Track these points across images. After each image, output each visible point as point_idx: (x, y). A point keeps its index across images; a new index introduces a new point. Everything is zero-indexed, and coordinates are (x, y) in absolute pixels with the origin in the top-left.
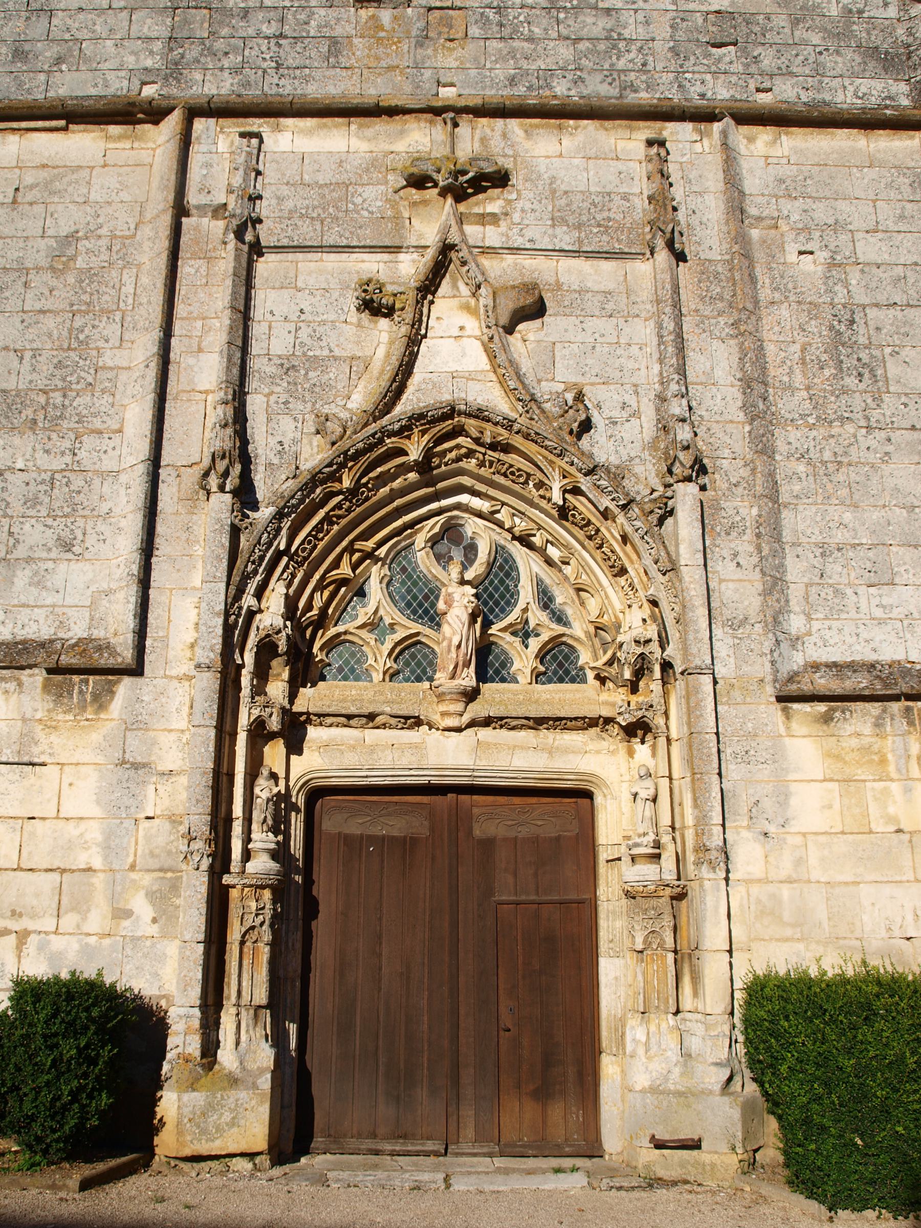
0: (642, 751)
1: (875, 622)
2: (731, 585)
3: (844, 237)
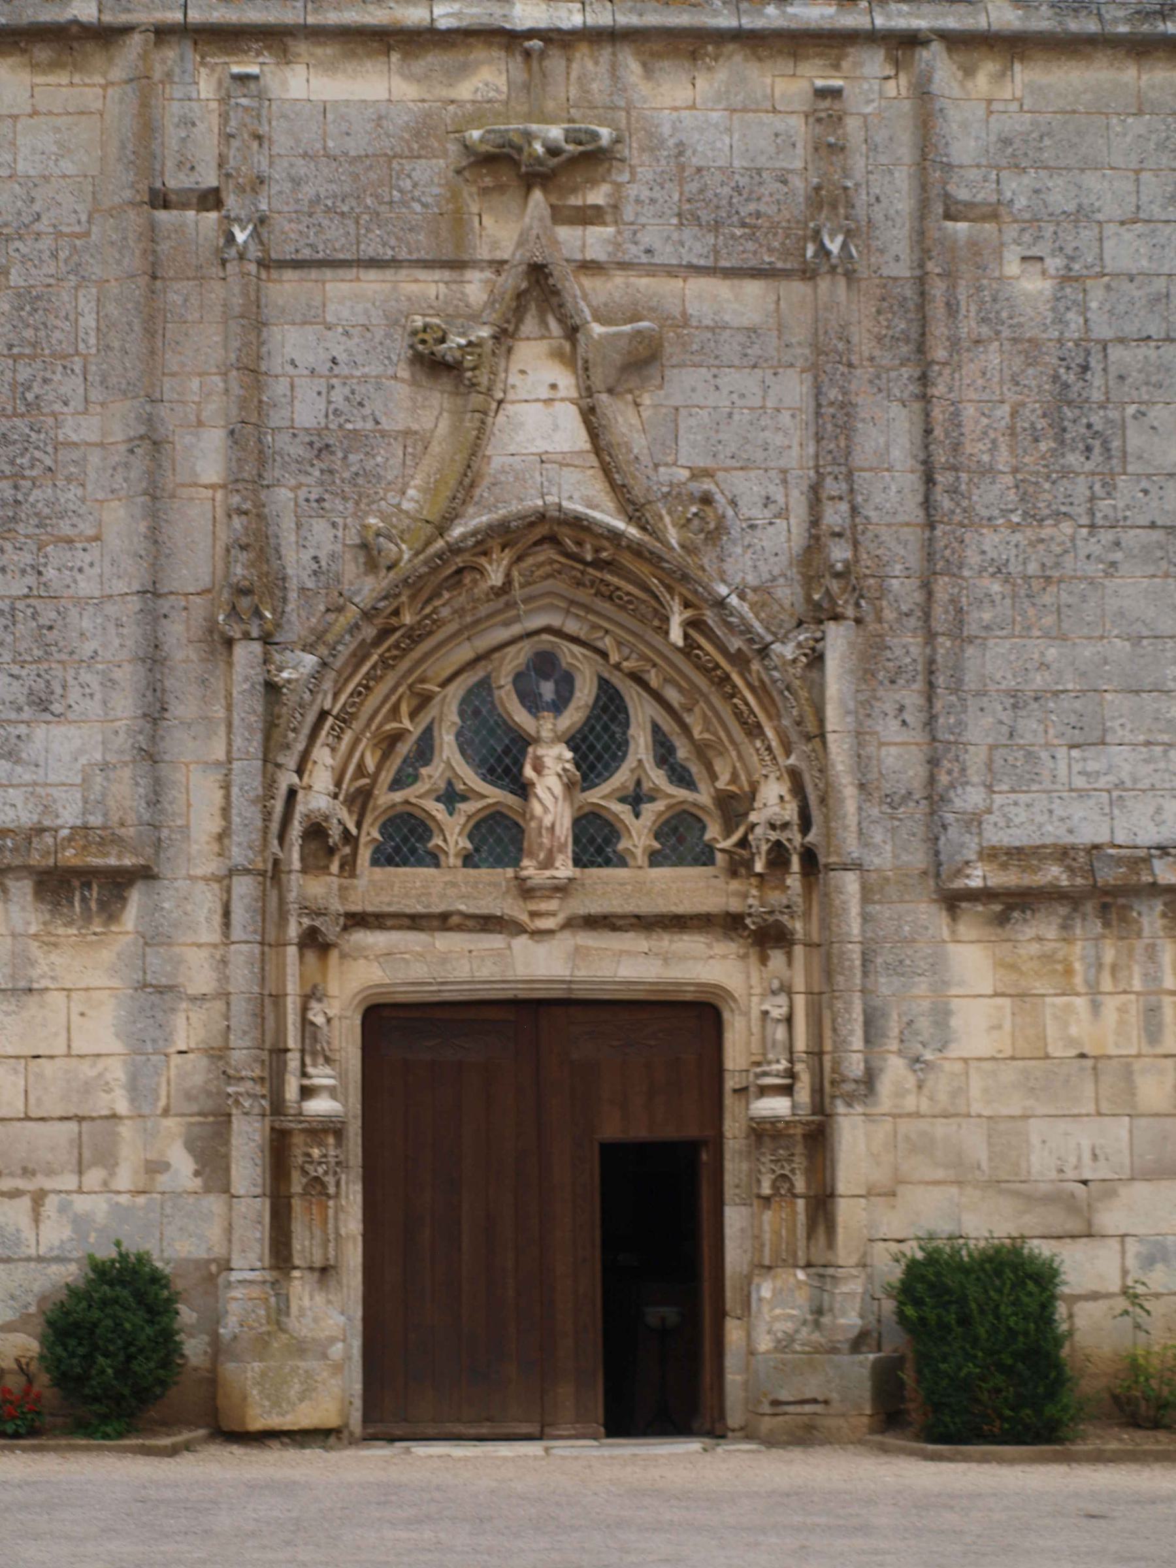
0: (777, 958)
1: (1074, 794)
2: (893, 750)
3: (1088, 234)
